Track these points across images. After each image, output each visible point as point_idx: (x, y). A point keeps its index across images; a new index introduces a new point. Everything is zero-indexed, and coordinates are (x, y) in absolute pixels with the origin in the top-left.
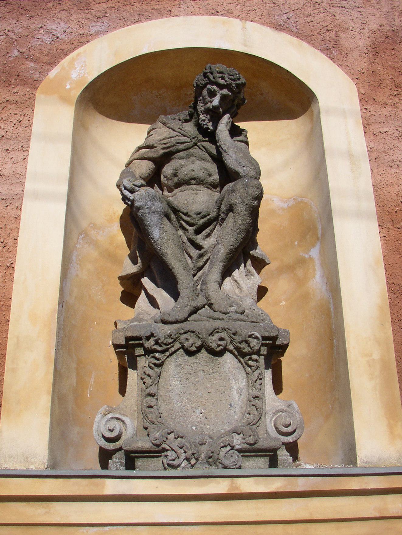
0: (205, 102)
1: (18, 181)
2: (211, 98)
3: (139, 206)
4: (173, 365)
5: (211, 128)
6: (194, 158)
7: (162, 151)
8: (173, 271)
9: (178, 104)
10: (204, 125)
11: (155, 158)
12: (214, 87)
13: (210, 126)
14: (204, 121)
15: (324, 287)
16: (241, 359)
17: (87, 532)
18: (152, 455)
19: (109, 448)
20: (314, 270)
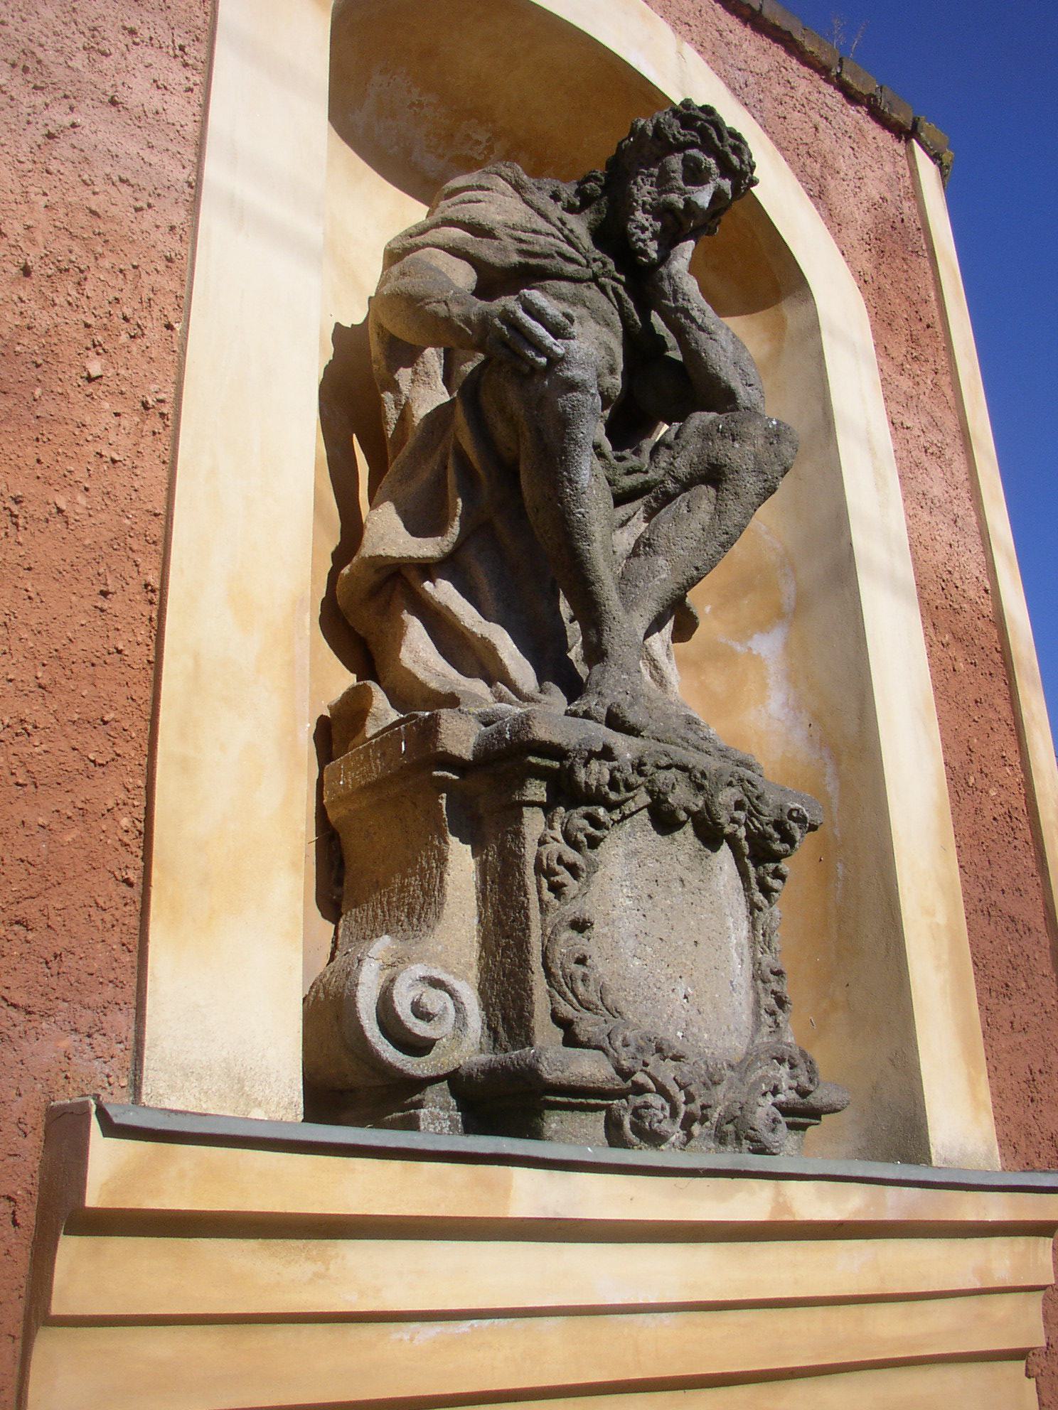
0: (663, 182)
1: (173, 148)
2: (687, 182)
3: (578, 379)
4: (621, 851)
5: (654, 255)
6: (584, 311)
7: (516, 259)
8: (596, 588)
9: (440, 151)
10: (640, 240)
11: (491, 266)
12: (712, 161)
13: (652, 249)
14: (644, 229)
15: (799, 735)
16: (752, 869)
17: (412, 1339)
18: (592, 1101)
19: (412, 1072)
20: (764, 686)
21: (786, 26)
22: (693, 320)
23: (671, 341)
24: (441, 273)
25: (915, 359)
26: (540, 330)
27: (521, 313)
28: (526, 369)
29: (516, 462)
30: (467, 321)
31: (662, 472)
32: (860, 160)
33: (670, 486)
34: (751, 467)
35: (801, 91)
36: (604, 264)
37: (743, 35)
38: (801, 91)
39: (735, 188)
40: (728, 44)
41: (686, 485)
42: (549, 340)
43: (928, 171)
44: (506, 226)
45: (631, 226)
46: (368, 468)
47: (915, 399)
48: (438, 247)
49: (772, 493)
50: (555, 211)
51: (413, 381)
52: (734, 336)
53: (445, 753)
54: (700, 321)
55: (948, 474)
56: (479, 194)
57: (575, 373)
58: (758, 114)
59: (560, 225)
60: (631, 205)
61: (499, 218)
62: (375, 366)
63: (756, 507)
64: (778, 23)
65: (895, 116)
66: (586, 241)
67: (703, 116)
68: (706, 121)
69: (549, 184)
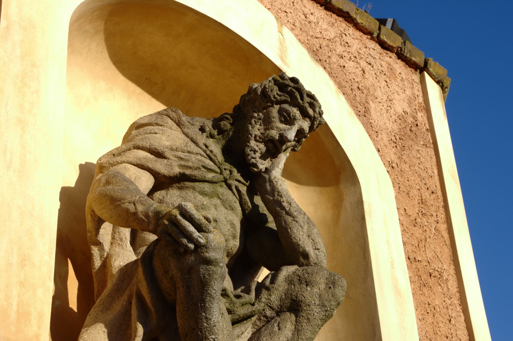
3: (213, 258)
14: (255, 152)
21: (346, 8)
22: (283, 208)
23: (270, 218)
24: (132, 183)
25: (423, 214)
26: (191, 228)
27: (179, 217)
28: (182, 250)
29: (174, 302)
30: (147, 215)
31: (263, 304)
32: (391, 89)
33: (269, 313)
34: (317, 303)
35: (355, 48)
36: (231, 172)
37: (319, 16)
38: (355, 48)
39: (311, 128)
40: (310, 22)
41: (279, 313)
42: (196, 234)
43: (433, 89)
44: (172, 149)
45: (248, 150)
46: (78, 284)
47: (423, 241)
48: (131, 163)
49: (330, 318)
50: (202, 139)
51: (112, 244)
52: (308, 219)
53: (98, 240)
54: (288, 209)
55: (445, 289)
56: (156, 128)
57: (211, 255)
58: (327, 66)
59: (204, 147)
60: (248, 137)
61: (168, 143)
62: (89, 234)
63: (320, 327)
64: (341, 7)
65: (413, 59)
66: (220, 158)
67: (292, 84)
68: (294, 88)
69: (199, 121)
